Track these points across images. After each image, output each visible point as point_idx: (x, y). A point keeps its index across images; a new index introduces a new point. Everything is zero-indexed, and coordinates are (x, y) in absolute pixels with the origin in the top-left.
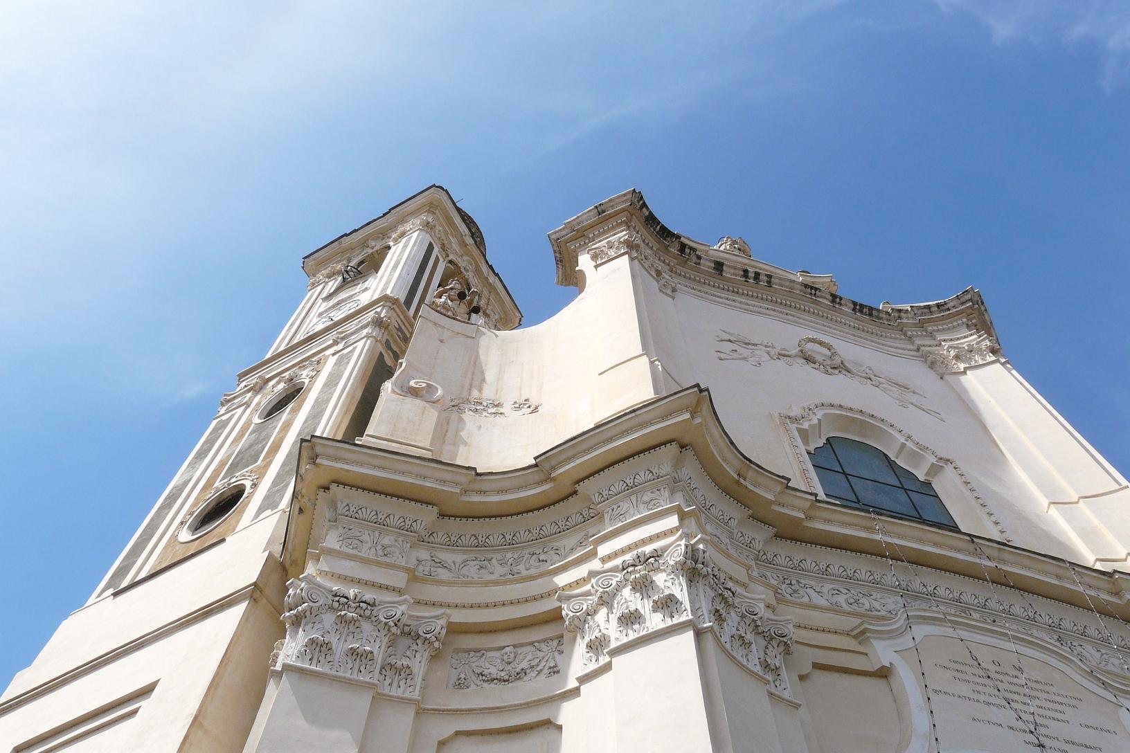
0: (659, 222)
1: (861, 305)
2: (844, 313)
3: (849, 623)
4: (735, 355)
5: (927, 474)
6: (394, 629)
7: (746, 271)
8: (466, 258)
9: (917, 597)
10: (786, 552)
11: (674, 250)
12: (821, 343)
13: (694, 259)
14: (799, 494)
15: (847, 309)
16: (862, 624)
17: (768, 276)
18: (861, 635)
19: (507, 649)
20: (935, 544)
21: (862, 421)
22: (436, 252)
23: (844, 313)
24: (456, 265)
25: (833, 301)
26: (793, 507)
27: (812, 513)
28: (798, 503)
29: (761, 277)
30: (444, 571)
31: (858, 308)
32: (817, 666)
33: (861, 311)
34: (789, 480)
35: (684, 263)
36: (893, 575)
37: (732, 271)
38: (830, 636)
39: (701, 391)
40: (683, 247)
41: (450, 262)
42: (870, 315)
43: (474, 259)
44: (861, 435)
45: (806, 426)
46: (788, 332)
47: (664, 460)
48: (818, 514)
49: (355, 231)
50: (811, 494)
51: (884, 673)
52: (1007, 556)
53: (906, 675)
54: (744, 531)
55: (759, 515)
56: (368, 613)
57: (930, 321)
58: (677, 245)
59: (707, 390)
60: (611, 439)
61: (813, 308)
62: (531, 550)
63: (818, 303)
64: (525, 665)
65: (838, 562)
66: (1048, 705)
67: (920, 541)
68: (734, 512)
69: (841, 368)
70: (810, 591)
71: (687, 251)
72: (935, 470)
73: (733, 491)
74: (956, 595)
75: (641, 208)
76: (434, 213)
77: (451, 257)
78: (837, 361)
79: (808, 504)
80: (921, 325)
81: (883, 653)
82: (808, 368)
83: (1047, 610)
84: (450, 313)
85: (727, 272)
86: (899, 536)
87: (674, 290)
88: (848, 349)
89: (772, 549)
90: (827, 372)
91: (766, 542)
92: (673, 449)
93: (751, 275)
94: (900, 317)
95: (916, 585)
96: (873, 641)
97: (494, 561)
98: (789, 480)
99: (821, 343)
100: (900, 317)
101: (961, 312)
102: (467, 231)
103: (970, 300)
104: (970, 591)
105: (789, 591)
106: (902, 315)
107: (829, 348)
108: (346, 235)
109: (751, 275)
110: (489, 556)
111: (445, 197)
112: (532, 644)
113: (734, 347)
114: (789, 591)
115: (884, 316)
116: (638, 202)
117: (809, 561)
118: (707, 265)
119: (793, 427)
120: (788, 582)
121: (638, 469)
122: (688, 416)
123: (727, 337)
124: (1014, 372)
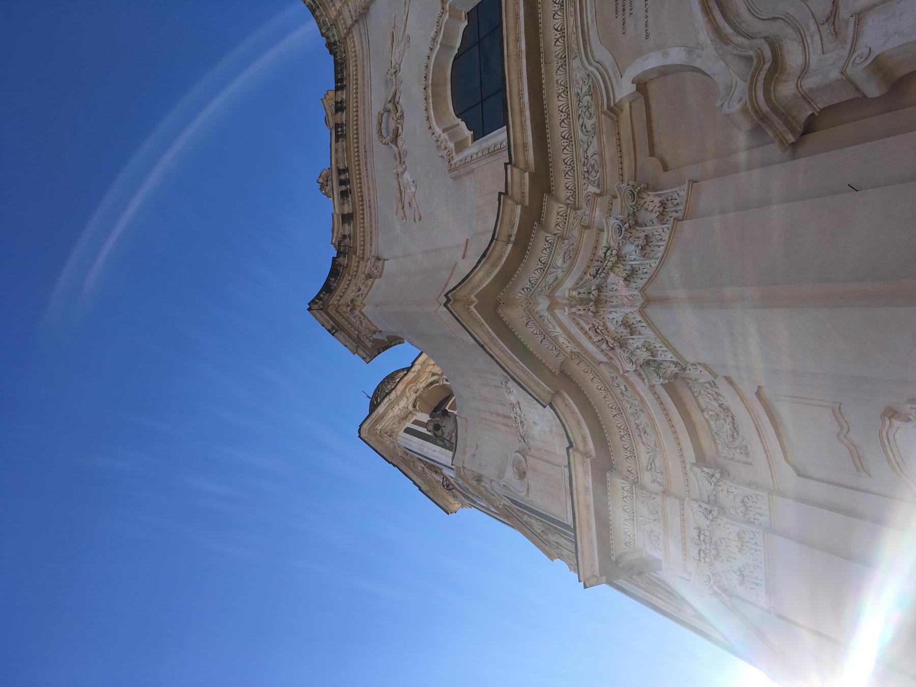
1: (337, 80)
3: (606, 122)
6: (715, 513)
8: (408, 394)
9: (567, 47)
11: (344, 261)
13: (347, 240)
15: (342, 95)
16: (604, 113)
18: (614, 111)
19: (707, 417)
20: (518, 40)
22: (409, 424)
24: (415, 401)
26: (522, 184)
27: (522, 165)
30: (656, 461)
32: (652, 154)
33: (341, 80)
34: (500, 194)
36: (554, 76)
38: (623, 142)
39: (449, 300)
40: (339, 253)
41: (414, 406)
43: (406, 387)
44: (446, 85)
45: (451, 145)
46: (378, 158)
47: (515, 315)
49: (415, 483)
50: (506, 169)
51: (642, 86)
53: (636, 69)
56: (707, 533)
59: (446, 295)
60: (513, 127)
62: (620, 396)
64: (716, 405)
65: (558, 130)
67: (518, 55)
70: (590, 153)
73: (523, 245)
74: (557, 7)
75: (321, 299)
77: (410, 407)
78: (390, 106)
79: (516, 170)
81: (625, 89)
82: (403, 135)
84: (454, 434)
85: (347, 209)
87: (378, 259)
88: (377, 101)
89: (563, 193)
90: (402, 117)
91: (557, 200)
93: (343, 188)
96: (617, 100)
97: (637, 422)
98: (500, 194)
102: (386, 400)
105: (593, 173)
108: (420, 489)
109: (343, 188)
110: (634, 426)
111: (365, 426)
112: (696, 398)
113: (407, 205)
114: (593, 173)
116: (321, 303)
117: (564, 156)
118: (347, 229)
119: (457, 158)
120: (586, 175)
121: (527, 333)
122: (472, 307)
123: (400, 210)
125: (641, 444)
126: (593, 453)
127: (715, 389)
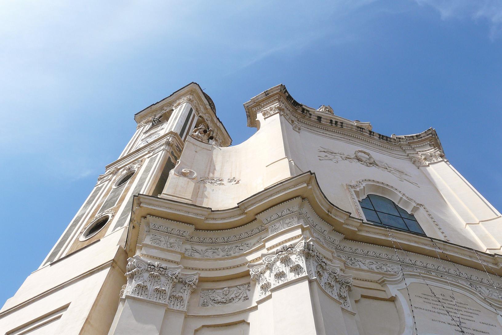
0: (293, 99)
1: (383, 136)
2: (375, 139)
3: (377, 277)
4: (326, 158)
5: (412, 211)
6: (175, 280)
7: (331, 121)
8: (207, 115)
9: (407, 265)
10: (349, 246)
11: (300, 111)
12: (365, 153)
13: (308, 115)
14: (355, 220)
15: (376, 138)
16: (383, 277)
17: (341, 123)
18: (383, 283)
19: (225, 289)
20: (415, 242)
21: (383, 187)
22: (194, 112)
23: (375, 139)
24: (203, 118)
25: (370, 134)
26: (352, 226)
27: (361, 228)
28: (354, 224)
29: (338, 123)
30: (197, 254)
31: (381, 137)
32: (363, 296)
33: (382, 138)
34: (350, 213)
35: (304, 117)
36: (397, 256)
37: (325, 120)
38: (369, 283)
39: (311, 174)
40: (303, 110)
41: (200, 116)
42: (387, 140)
43: (210, 115)
44: (382, 194)
46: (350, 148)
47: (295, 205)
48: (364, 228)
49: (158, 103)
50: (360, 220)
51: (393, 300)
52: (447, 248)
53: (402, 300)
54: (331, 236)
55: (337, 229)
56: (163, 273)
57: (413, 143)
58: (301, 109)
59: (314, 173)
60: (271, 195)
61: (361, 137)
62: (236, 245)
63: (363, 135)
64: (233, 296)
65: (372, 250)
66: (466, 313)
67: (409, 241)
68: (326, 228)
69: (374, 164)
70: (360, 263)
71: (305, 111)
72: (415, 209)
73: (326, 218)
74: (425, 265)
75: (285, 93)
76: (193, 95)
77: (200, 114)
78: (372, 161)
79: (359, 224)
80: (409, 144)
81: (392, 290)
82: (359, 164)
83: (465, 272)
84: (200, 139)
85: (323, 121)
86: (400, 239)
87: (299, 129)
88: (377, 155)
89: (343, 244)
90: (367, 166)
91: (340, 241)
92: (299, 200)
93: (334, 122)
94: (400, 141)
95: (407, 260)
96: (388, 285)
97: (219, 250)
98: (350, 213)
99: (365, 153)
100: (400, 141)
101: (427, 139)
102: (207, 103)
103: (431, 133)
104: (431, 263)
105: (351, 263)
106: (401, 140)
107: (368, 155)
108: (154, 105)
109: (334, 122)
110: (217, 247)
111: (198, 88)
112: (236, 286)
113: (326, 154)
114: (351, 263)
115: (393, 141)
116: (283, 90)
117: (359, 250)
118: (314, 118)
119: (352, 190)
120: (350, 259)
121: (284, 209)
122: (305, 185)
123: (323, 150)
124: (450, 165)
125: (207, 248)
126: (207, 222)
127: (242, 299)
